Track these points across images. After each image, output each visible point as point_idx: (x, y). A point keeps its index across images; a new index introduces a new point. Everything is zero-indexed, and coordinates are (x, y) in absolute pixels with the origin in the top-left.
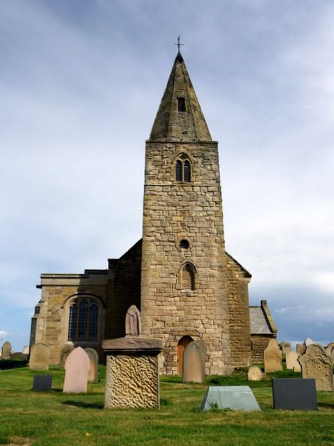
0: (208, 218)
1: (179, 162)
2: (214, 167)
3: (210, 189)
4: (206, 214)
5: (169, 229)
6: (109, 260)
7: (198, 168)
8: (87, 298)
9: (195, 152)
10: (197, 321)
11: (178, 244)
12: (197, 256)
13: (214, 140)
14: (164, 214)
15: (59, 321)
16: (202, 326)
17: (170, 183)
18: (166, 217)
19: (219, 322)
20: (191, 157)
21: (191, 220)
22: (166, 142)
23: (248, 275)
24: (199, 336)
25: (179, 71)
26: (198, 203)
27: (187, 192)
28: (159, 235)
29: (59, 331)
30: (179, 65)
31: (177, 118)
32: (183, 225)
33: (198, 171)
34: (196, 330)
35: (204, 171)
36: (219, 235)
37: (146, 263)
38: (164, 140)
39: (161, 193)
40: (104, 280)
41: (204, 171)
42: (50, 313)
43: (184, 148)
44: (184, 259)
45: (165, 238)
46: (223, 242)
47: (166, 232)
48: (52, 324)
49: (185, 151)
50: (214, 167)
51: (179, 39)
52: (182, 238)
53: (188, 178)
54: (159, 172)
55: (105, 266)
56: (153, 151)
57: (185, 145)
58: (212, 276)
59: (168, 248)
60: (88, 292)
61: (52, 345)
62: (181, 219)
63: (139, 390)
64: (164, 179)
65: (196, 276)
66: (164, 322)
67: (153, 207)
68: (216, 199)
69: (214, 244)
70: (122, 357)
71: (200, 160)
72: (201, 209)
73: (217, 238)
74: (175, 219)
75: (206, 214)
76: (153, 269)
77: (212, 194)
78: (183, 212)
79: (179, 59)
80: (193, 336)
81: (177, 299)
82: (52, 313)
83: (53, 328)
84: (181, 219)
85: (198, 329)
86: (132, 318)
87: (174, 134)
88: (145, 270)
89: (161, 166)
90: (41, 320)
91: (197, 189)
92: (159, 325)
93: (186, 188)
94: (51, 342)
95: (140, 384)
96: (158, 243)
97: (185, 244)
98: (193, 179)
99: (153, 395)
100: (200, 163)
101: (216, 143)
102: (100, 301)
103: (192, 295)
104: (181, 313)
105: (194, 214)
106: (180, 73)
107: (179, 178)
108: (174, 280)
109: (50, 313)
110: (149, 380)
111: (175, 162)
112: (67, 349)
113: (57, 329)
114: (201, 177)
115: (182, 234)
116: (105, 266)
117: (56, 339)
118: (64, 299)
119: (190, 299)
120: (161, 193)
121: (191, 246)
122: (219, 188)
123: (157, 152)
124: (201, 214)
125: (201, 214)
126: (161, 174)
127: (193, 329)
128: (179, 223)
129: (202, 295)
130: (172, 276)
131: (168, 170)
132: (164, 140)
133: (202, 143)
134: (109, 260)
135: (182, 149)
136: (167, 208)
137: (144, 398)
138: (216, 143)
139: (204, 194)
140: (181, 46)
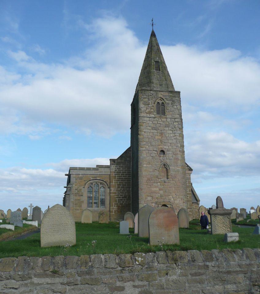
0: (175, 137)
1: (158, 103)
2: (178, 107)
3: (176, 120)
4: (174, 135)
5: (153, 143)
6: (110, 160)
7: (169, 108)
8: (99, 182)
9: (168, 97)
10: (170, 197)
11: (159, 152)
12: (170, 160)
13: (176, 89)
14: (151, 135)
15: (82, 196)
16: (172, 199)
17: (153, 116)
18: (152, 136)
19: (182, 197)
20: (165, 100)
21: (166, 138)
22: (151, 90)
23: (191, 170)
24: (171, 205)
25: (154, 44)
26: (170, 128)
27: (163, 121)
28: (147, 147)
29: (83, 202)
30: (154, 39)
31: (155, 77)
32: (161, 141)
33: (169, 109)
34: (169, 201)
35: (172, 109)
36: (182, 148)
37: (141, 163)
38: (149, 88)
39: (148, 122)
40: (107, 171)
41: (172, 109)
42: (77, 191)
43: (161, 94)
44: (162, 161)
45: (151, 148)
46: (184, 152)
47: (152, 145)
48: (78, 198)
49: (162, 96)
50: (178, 107)
51: (152, 21)
52: (161, 149)
53: (164, 113)
54: (147, 109)
55: (108, 163)
56: (143, 95)
57: (162, 93)
58: (178, 171)
59: (153, 155)
60: (99, 179)
61: (78, 210)
62: (160, 137)
63: (224, 228)
64: (150, 113)
65: (169, 171)
66: (152, 197)
67: (144, 130)
68: (180, 127)
69: (179, 153)
70: (217, 216)
71: (170, 102)
72: (171, 132)
73: (180, 149)
74: (156, 137)
75: (156, 132)
76: (145, 167)
77: (177, 123)
78: (162, 134)
79: (153, 35)
80: (168, 204)
81: (159, 184)
82: (78, 191)
83: (79, 200)
84: (160, 137)
85: (170, 201)
86: (220, 201)
87: (155, 86)
88: (140, 168)
89: (148, 105)
90: (72, 195)
91: (169, 120)
92: (149, 198)
93: (163, 119)
94: (78, 208)
95: (225, 226)
96: (147, 152)
97: (163, 152)
98: (167, 113)
99: (230, 230)
100: (170, 104)
101: (179, 93)
102: (106, 184)
103: (167, 181)
104: (161, 192)
105: (167, 135)
106: (155, 45)
107: (158, 113)
108: (156, 173)
109: (77, 191)
110: (228, 225)
111: (156, 103)
112: (102, 212)
113: (81, 201)
114: (171, 113)
115: (161, 147)
116: (108, 163)
117: (81, 206)
118: (84, 183)
119: (166, 184)
120: (148, 122)
121: (166, 154)
122: (182, 120)
123: (145, 96)
124: (172, 135)
125: (172, 135)
126: (148, 110)
127: (168, 201)
128: (159, 140)
129: (172, 182)
130: (156, 171)
131: (152, 108)
132: (149, 88)
133: (171, 92)
134: (110, 160)
135: (160, 95)
136: (152, 131)
137: (227, 231)
138: (179, 93)
139: (173, 123)
140: (154, 25)
